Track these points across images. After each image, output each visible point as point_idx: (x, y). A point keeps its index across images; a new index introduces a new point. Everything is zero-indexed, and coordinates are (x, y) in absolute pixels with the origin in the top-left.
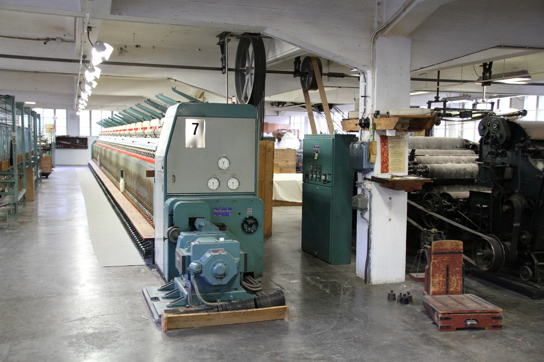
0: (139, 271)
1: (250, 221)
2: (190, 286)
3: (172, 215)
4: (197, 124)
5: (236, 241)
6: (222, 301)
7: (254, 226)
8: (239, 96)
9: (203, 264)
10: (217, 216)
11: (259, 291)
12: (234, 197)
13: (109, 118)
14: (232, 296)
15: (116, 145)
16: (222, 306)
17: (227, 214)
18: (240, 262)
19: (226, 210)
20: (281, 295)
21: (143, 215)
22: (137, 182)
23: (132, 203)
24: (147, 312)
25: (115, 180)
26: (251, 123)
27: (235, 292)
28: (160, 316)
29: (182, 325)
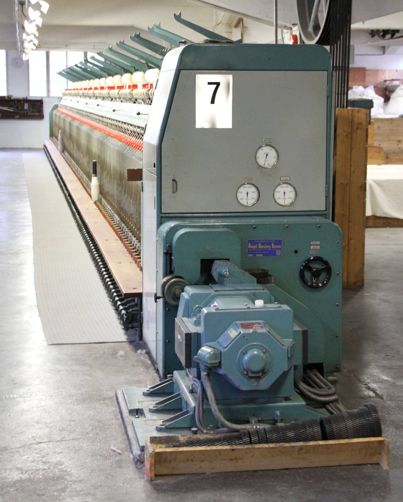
0: (114, 354)
1: (316, 266)
2: (199, 390)
3: (171, 255)
4: (218, 84)
5: (286, 307)
6: (259, 421)
7: (323, 276)
8: (304, 26)
9: (223, 351)
10: (254, 255)
11: (332, 402)
12: (285, 220)
13: (76, 66)
14: (278, 413)
15: (88, 115)
16: (257, 432)
17: (272, 253)
18: (293, 347)
20: (374, 415)
21: (127, 247)
22: (119, 185)
23: (109, 223)
24: (121, 438)
25: (85, 178)
26: (315, 83)
27: (284, 404)
28: (143, 449)
29: (183, 468)
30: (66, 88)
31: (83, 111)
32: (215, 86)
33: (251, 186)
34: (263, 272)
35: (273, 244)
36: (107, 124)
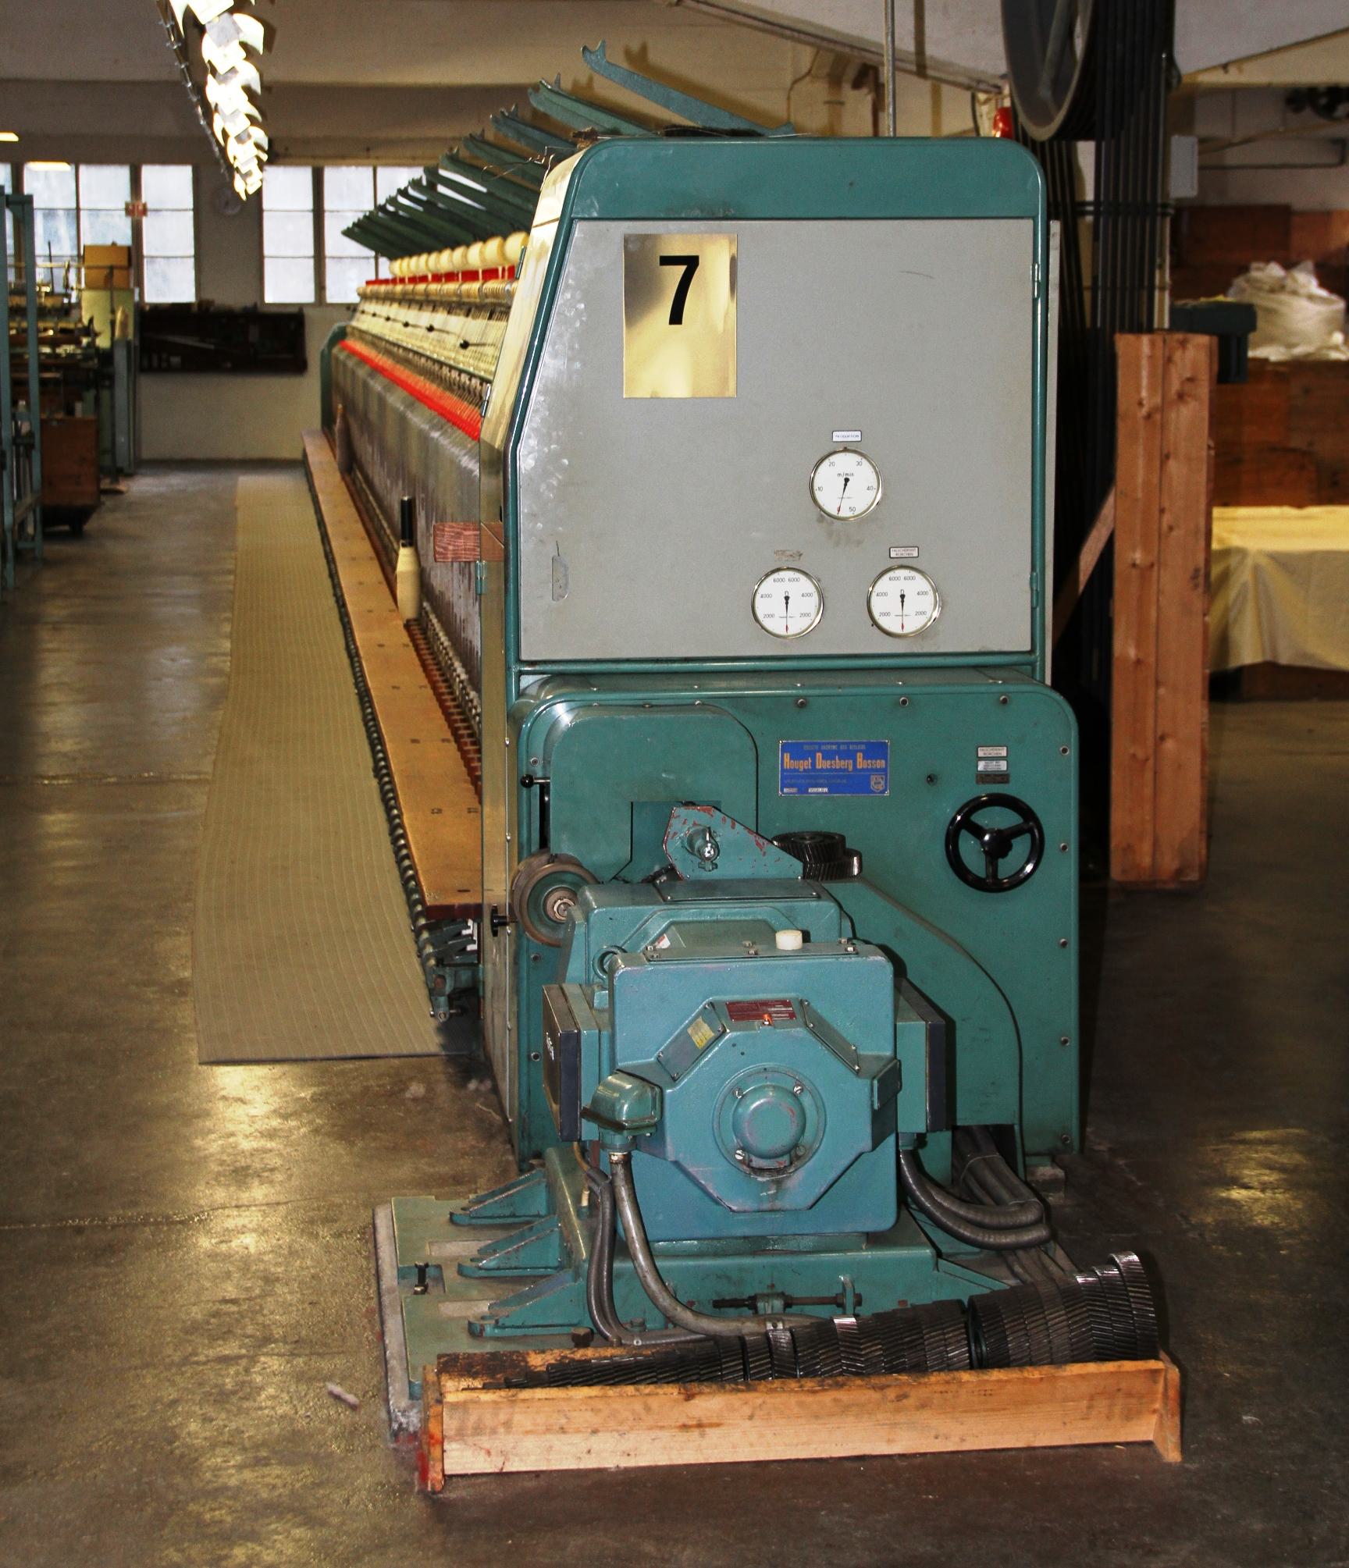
10: (803, 790)
17: (857, 783)
19: (850, 755)
30: (373, 277)
31: (399, 346)
32: (681, 269)
33: (798, 575)
34: (828, 841)
35: (860, 755)
36: (450, 386)
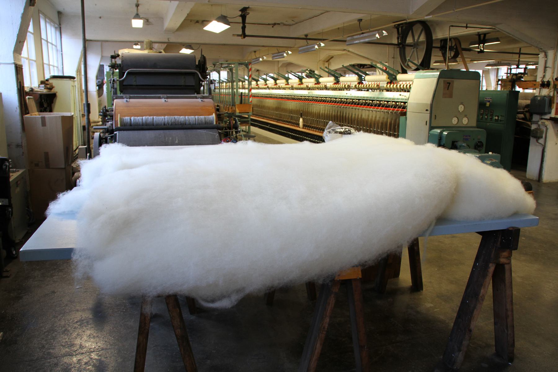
4: (450, 83)
